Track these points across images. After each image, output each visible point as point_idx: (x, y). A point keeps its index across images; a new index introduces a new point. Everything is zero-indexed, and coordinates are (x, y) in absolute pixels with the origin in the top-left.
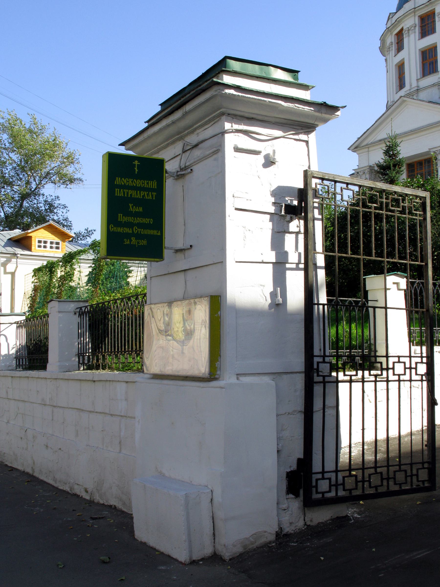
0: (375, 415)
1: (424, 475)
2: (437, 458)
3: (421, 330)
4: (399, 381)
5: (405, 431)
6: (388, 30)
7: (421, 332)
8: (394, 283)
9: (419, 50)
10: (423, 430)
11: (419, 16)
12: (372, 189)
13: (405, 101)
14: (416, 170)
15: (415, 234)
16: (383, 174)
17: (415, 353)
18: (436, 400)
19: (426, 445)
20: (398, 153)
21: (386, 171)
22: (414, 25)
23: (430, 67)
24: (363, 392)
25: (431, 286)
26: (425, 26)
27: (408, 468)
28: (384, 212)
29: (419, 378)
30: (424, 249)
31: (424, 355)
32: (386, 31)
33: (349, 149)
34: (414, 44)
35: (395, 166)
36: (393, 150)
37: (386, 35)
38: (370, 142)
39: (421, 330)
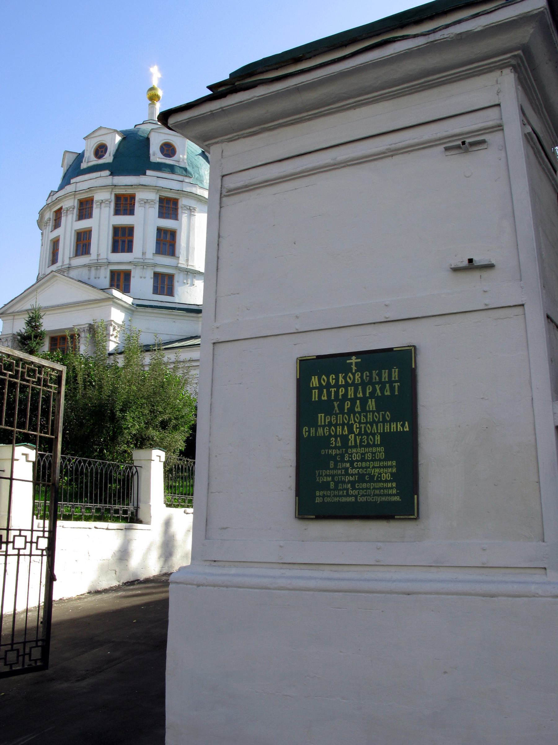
1: (37, 653)
2: (52, 635)
3: (45, 503)
4: (19, 555)
5: (21, 608)
6: (48, 206)
7: (45, 506)
8: (23, 454)
10: (39, 606)
12: (9, 356)
13: (56, 276)
14: (58, 344)
15: (48, 407)
16: (23, 344)
17: (38, 527)
18: (55, 576)
19: (41, 622)
20: (40, 325)
21: (27, 340)
23: (83, 248)
24: (5, 571)
25: (59, 460)
26: (83, 209)
27: (20, 647)
28: (18, 381)
29: (39, 552)
30: (55, 422)
31: (47, 529)
34: (71, 224)
35: (36, 337)
36: (35, 321)
37: (45, 211)
39: (45, 503)
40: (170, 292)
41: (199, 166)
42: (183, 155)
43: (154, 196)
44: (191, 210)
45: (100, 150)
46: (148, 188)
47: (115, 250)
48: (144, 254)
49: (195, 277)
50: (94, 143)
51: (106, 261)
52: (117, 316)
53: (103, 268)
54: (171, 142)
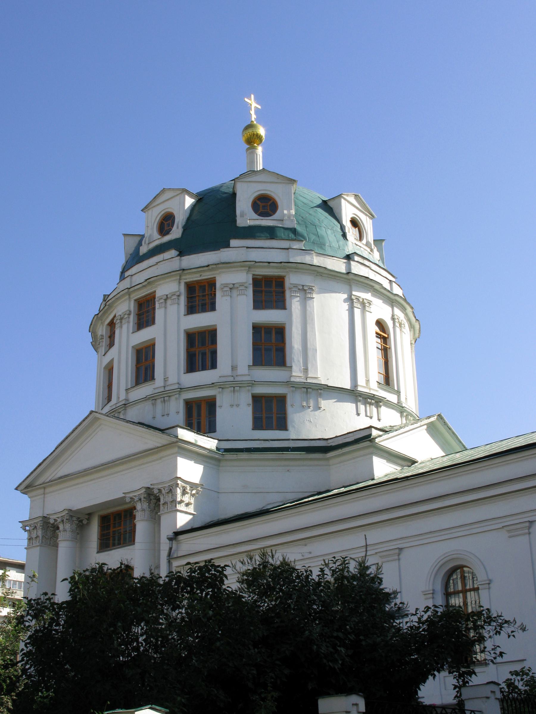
0: (466, 712)
6: (98, 318)
9: (133, 347)
11: (135, 300)
13: (99, 419)
22: (128, 312)
32: (95, 318)
33: (16, 489)
34: (129, 338)
38: (48, 480)
40: (282, 424)
41: (317, 222)
42: (289, 209)
43: (244, 278)
44: (305, 292)
45: (166, 222)
46: (233, 265)
47: (191, 368)
48: (234, 368)
49: (320, 395)
50: (156, 214)
51: (176, 386)
52: (190, 471)
53: (173, 398)
54: (268, 193)
